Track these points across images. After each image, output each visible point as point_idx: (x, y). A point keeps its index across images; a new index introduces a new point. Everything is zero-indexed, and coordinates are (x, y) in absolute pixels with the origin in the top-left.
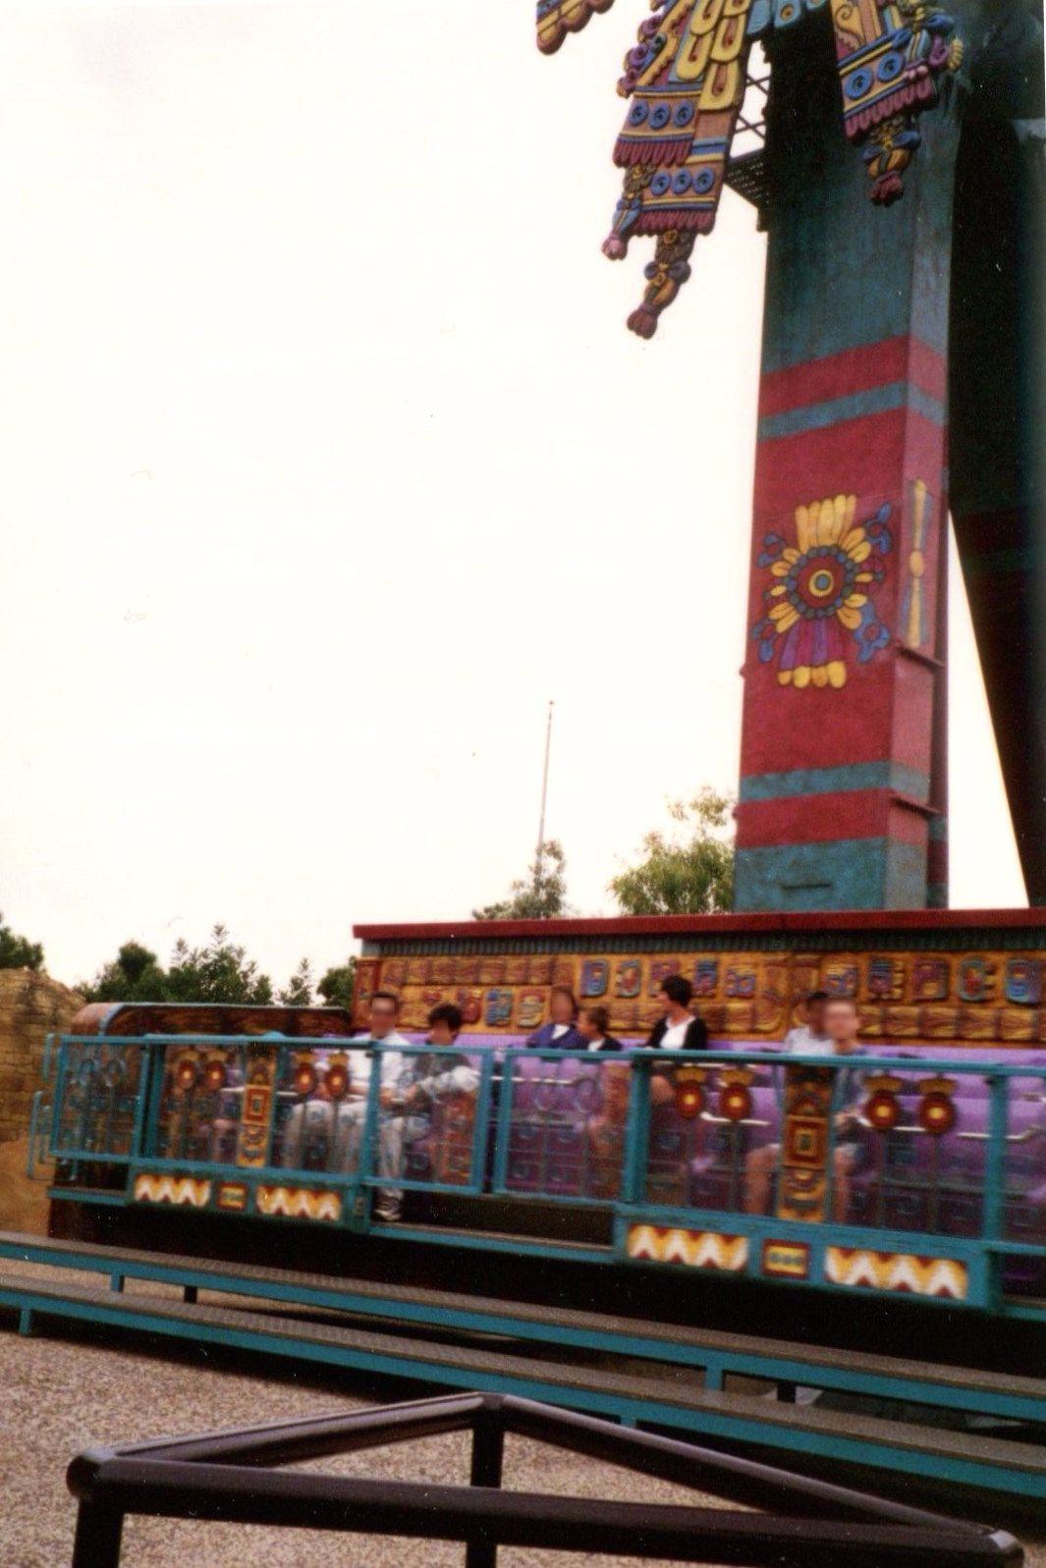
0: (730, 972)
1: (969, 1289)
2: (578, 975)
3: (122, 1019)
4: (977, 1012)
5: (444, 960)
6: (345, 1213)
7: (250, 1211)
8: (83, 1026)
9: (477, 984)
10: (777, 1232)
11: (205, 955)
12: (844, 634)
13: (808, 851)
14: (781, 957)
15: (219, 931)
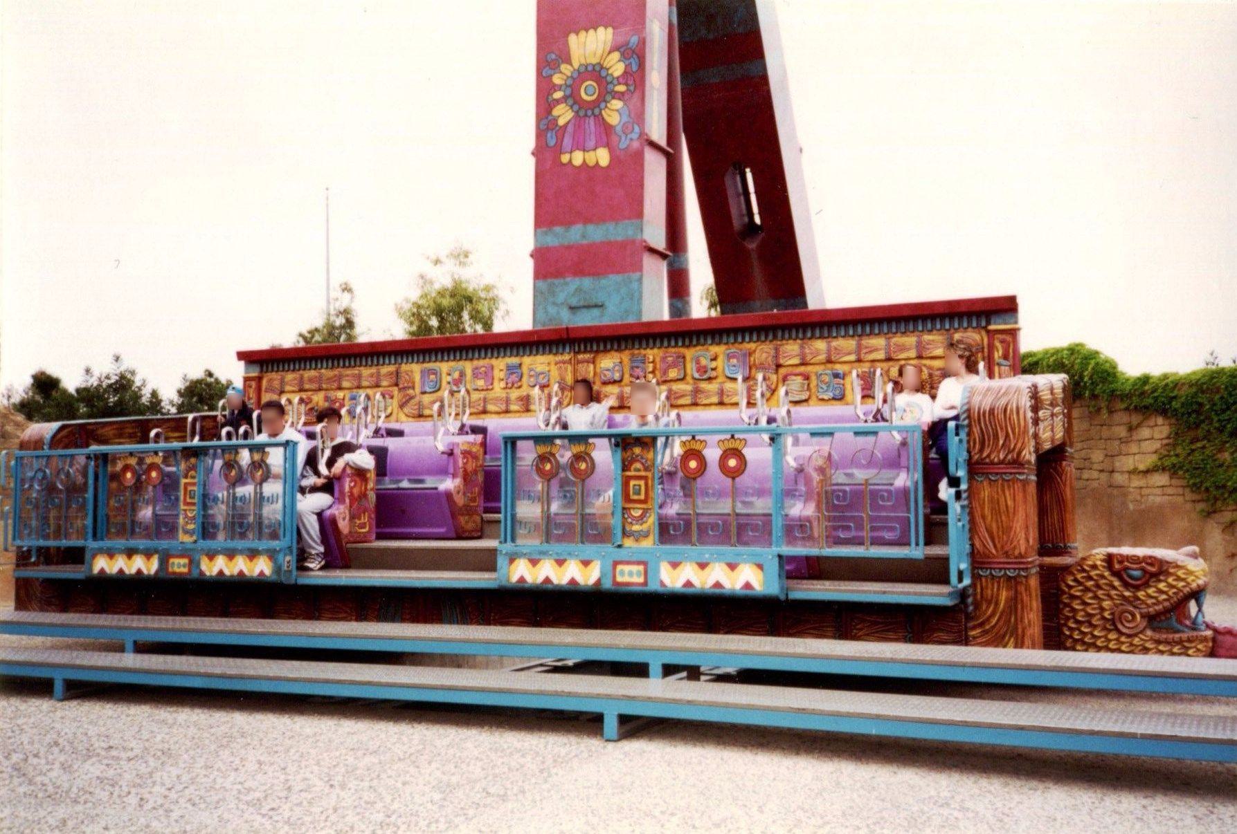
0: (531, 370)
1: (765, 582)
2: (417, 377)
3: (59, 436)
4: (703, 385)
5: (313, 373)
6: (278, 570)
7: (195, 574)
8: (29, 442)
9: (340, 388)
10: (622, 554)
11: (108, 377)
12: (607, 129)
13: (587, 282)
14: (566, 357)
15: (117, 359)
